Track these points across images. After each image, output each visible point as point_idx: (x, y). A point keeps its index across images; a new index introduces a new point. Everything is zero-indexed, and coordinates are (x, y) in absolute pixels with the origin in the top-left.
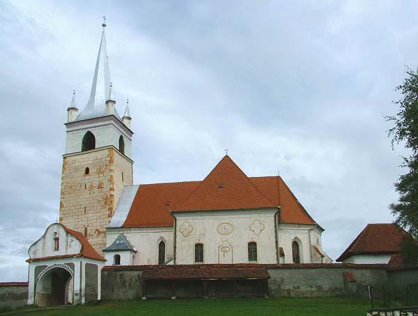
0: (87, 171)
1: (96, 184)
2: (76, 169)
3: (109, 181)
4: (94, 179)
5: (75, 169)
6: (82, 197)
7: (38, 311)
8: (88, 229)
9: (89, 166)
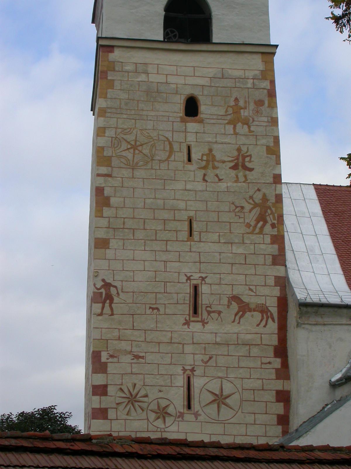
0: (192, 107)
1: (224, 152)
2: (153, 94)
3: (268, 148)
4: (210, 133)
5: (148, 92)
6: (180, 186)
7: (73, 440)
8: (204, 289)
9: (196, 92)
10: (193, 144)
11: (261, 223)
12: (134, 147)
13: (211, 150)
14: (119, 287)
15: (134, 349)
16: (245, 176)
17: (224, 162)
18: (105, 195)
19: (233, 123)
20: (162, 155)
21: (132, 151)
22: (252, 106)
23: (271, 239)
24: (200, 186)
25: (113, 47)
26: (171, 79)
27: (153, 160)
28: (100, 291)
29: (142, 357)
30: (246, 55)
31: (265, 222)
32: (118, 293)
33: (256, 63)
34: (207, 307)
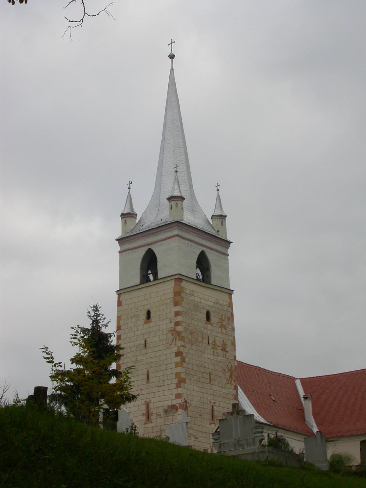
10: (210, 336)
11: (231, 379)
12: (192, 334)
13: (215, 340)
14: (190, 403)
15: (195, 434)
16: (226, 355)
17: (219, 346)
18: (184, 356)
19: (221, 327)
20: (200, 339)
21: (191, 335)
22: (226, 320)
23: (234, 387)
24: (212, 357)
25: (182, 279)
26: (202, 301)
27: (190, 334)
28: (183, 404)
29: (197, 438)
30: (224, 293)
31: (232, 379)
32: (189, 406)
33: (226, 296)
34: (216, 417)
